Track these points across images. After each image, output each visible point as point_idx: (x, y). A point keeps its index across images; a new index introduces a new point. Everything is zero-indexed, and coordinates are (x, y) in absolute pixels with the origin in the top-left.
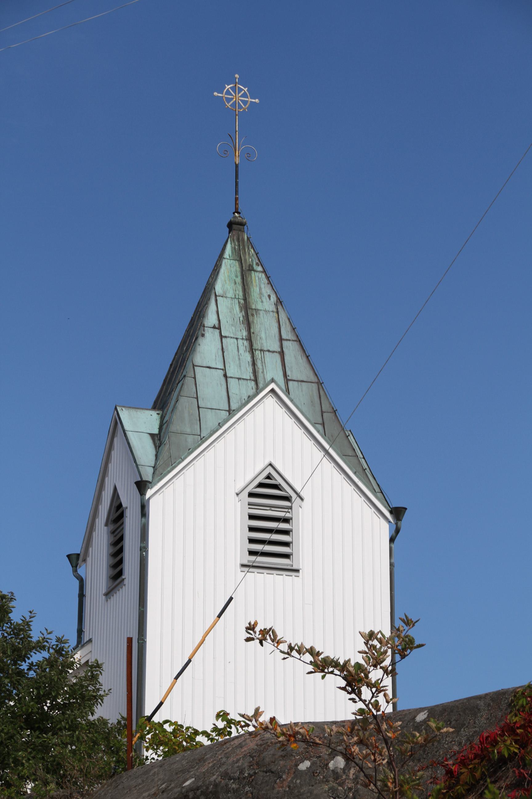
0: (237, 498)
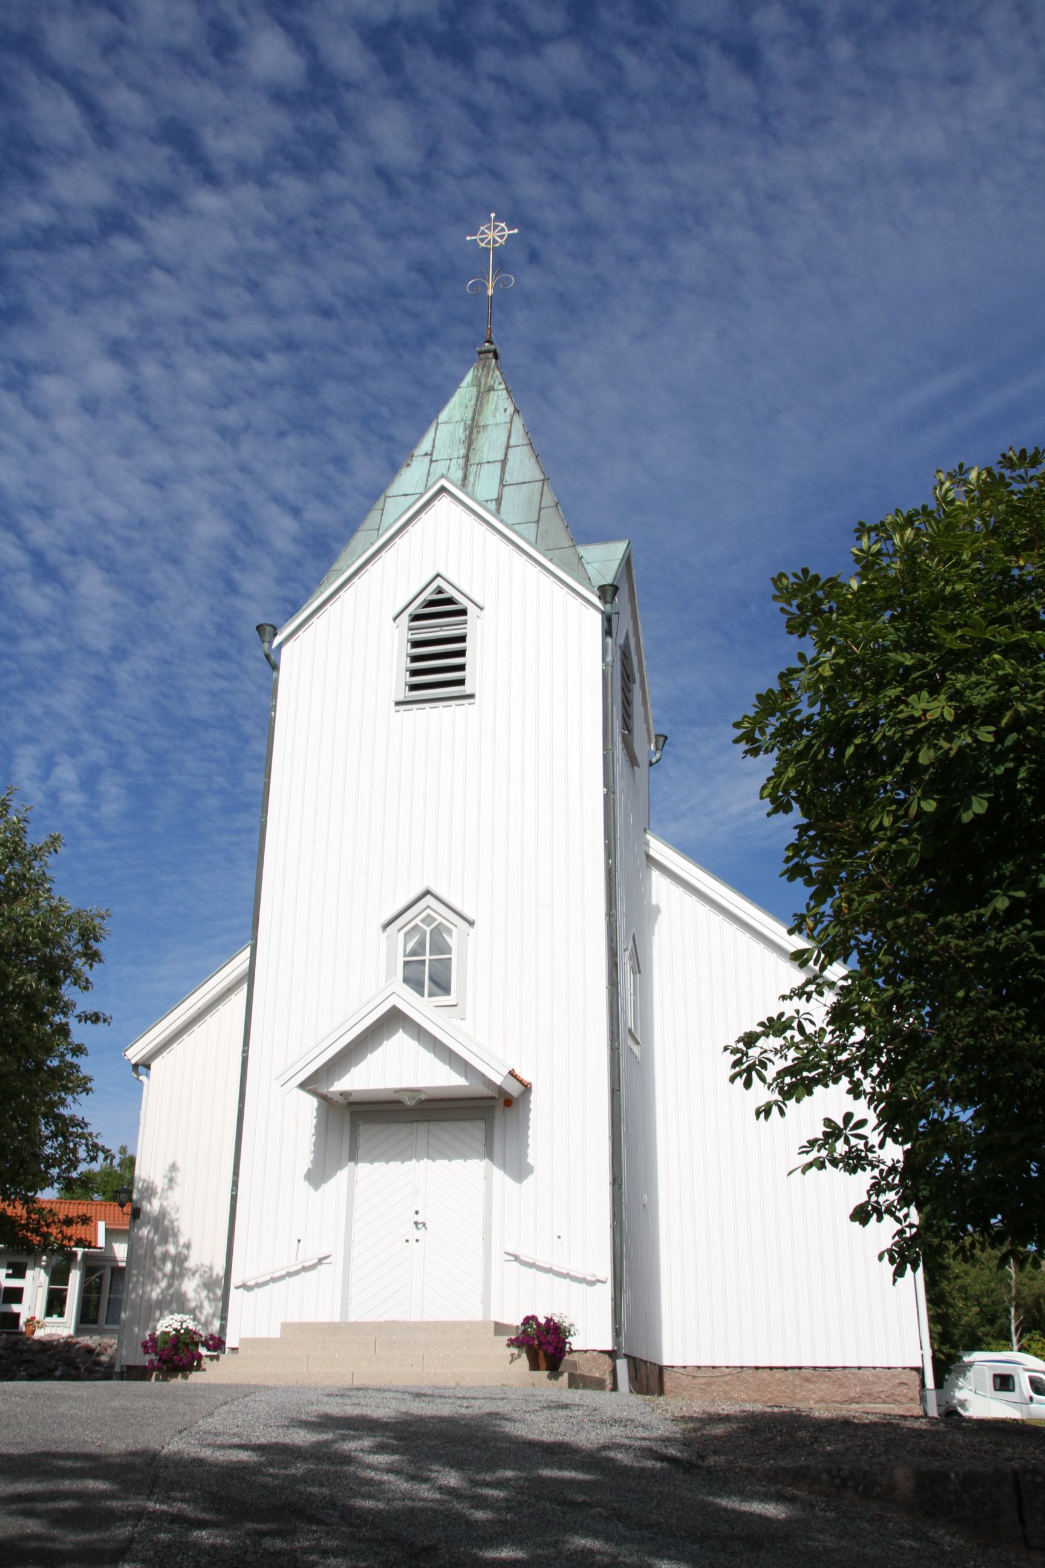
0: (395, 625)
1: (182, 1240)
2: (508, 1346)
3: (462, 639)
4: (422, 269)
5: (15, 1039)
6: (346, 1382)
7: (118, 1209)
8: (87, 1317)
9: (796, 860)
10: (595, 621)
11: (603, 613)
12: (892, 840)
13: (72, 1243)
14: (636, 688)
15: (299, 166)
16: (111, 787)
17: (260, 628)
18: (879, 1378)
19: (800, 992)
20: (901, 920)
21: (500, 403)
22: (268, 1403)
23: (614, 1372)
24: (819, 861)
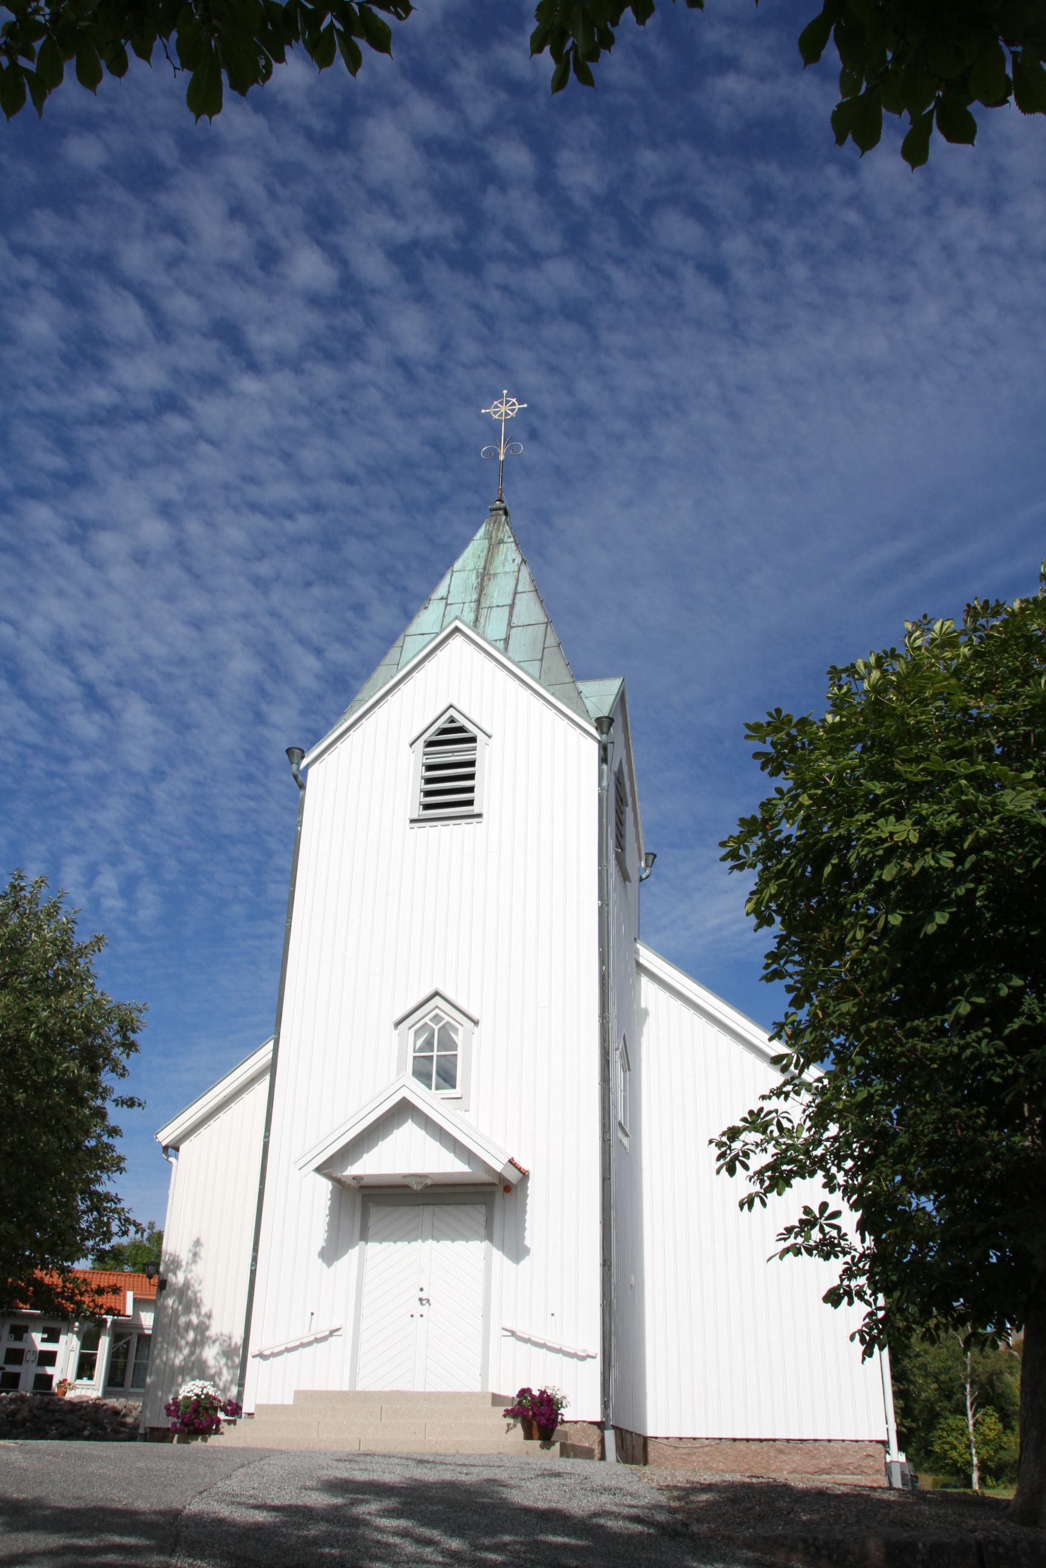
2: (505, 1416)
3: (472, 764)
4: (435, 443)
5: (58, 1121)
6: (354, 1448)
7: (146, 1280)
8: (114, 1380)
9: (774, 966)
10: (591, 750)
11: (599, 742)
12: (864, 950)
13: (103, 1311)
14: (629, 810)
15: (329, 357)
16: (148, 894)
18: (847, 1450)
19: (778, 1092)
20: (874, 1025)
21: (509, 555)
22: (282, 1467)
23: (602, 1442)
24: (798, 969)
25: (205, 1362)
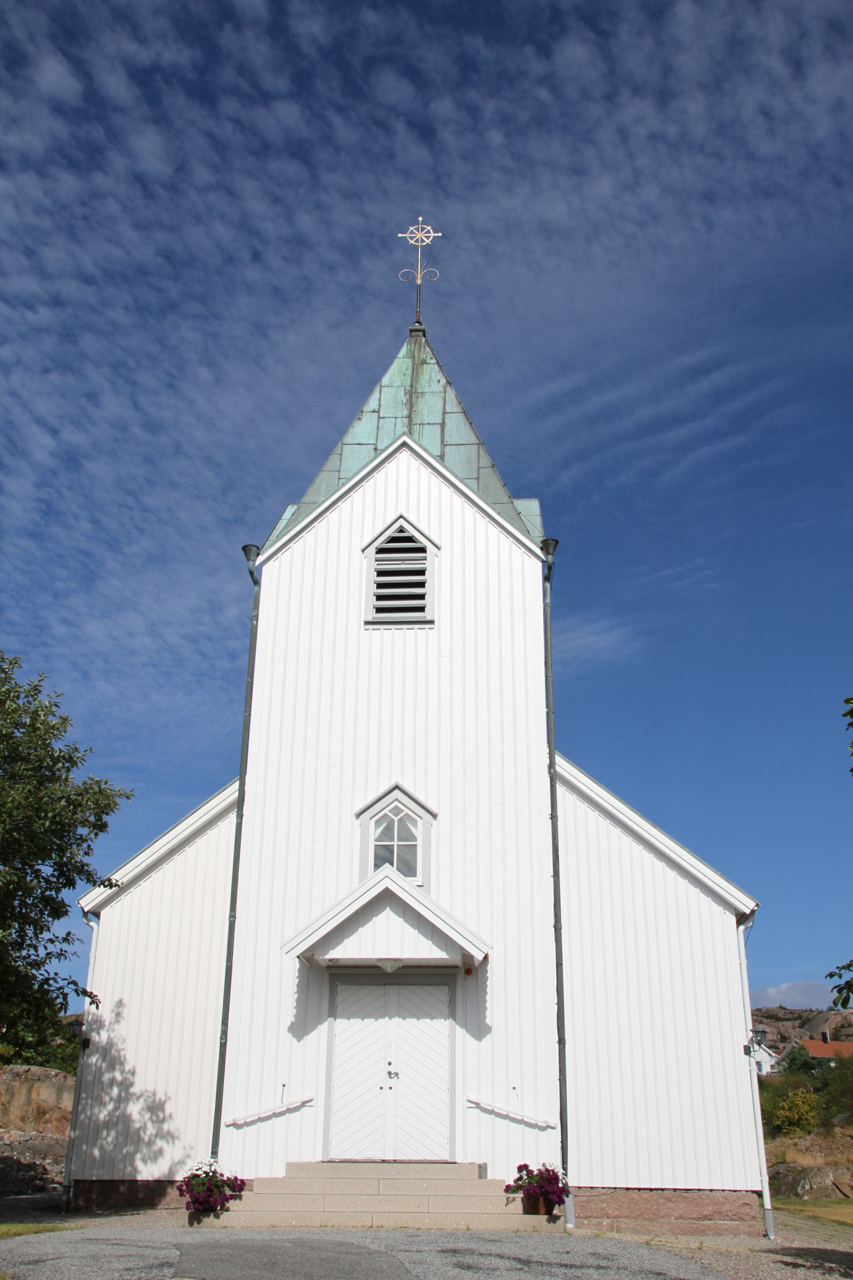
0: (364, 556)
1: (128, 1068)
3: (422, 572)
4: (168, 255)
10: (535, 569)
11: (543, 561)
15: (72, 165)
17: (246, 549)
18: (727, 1199)
21: (432, 377)
25: (130, 1116)
